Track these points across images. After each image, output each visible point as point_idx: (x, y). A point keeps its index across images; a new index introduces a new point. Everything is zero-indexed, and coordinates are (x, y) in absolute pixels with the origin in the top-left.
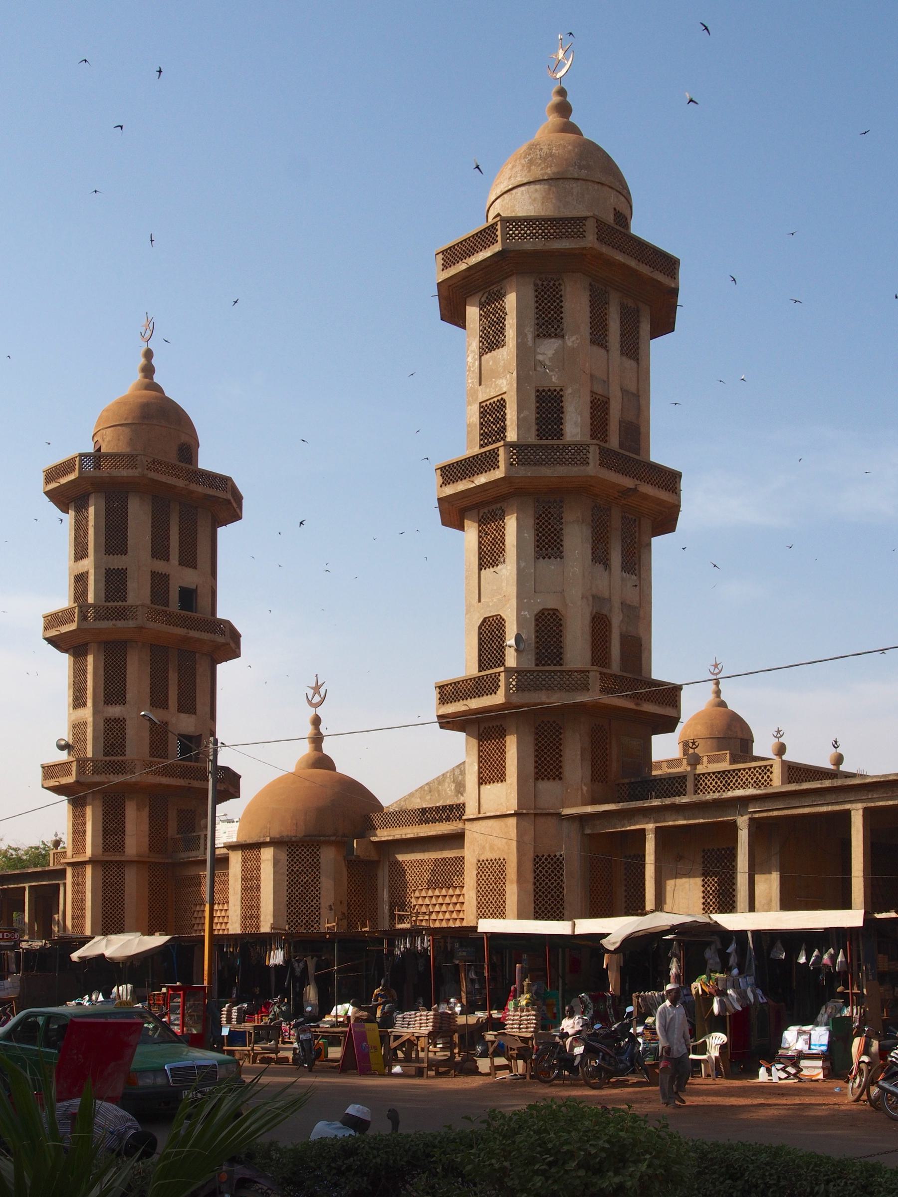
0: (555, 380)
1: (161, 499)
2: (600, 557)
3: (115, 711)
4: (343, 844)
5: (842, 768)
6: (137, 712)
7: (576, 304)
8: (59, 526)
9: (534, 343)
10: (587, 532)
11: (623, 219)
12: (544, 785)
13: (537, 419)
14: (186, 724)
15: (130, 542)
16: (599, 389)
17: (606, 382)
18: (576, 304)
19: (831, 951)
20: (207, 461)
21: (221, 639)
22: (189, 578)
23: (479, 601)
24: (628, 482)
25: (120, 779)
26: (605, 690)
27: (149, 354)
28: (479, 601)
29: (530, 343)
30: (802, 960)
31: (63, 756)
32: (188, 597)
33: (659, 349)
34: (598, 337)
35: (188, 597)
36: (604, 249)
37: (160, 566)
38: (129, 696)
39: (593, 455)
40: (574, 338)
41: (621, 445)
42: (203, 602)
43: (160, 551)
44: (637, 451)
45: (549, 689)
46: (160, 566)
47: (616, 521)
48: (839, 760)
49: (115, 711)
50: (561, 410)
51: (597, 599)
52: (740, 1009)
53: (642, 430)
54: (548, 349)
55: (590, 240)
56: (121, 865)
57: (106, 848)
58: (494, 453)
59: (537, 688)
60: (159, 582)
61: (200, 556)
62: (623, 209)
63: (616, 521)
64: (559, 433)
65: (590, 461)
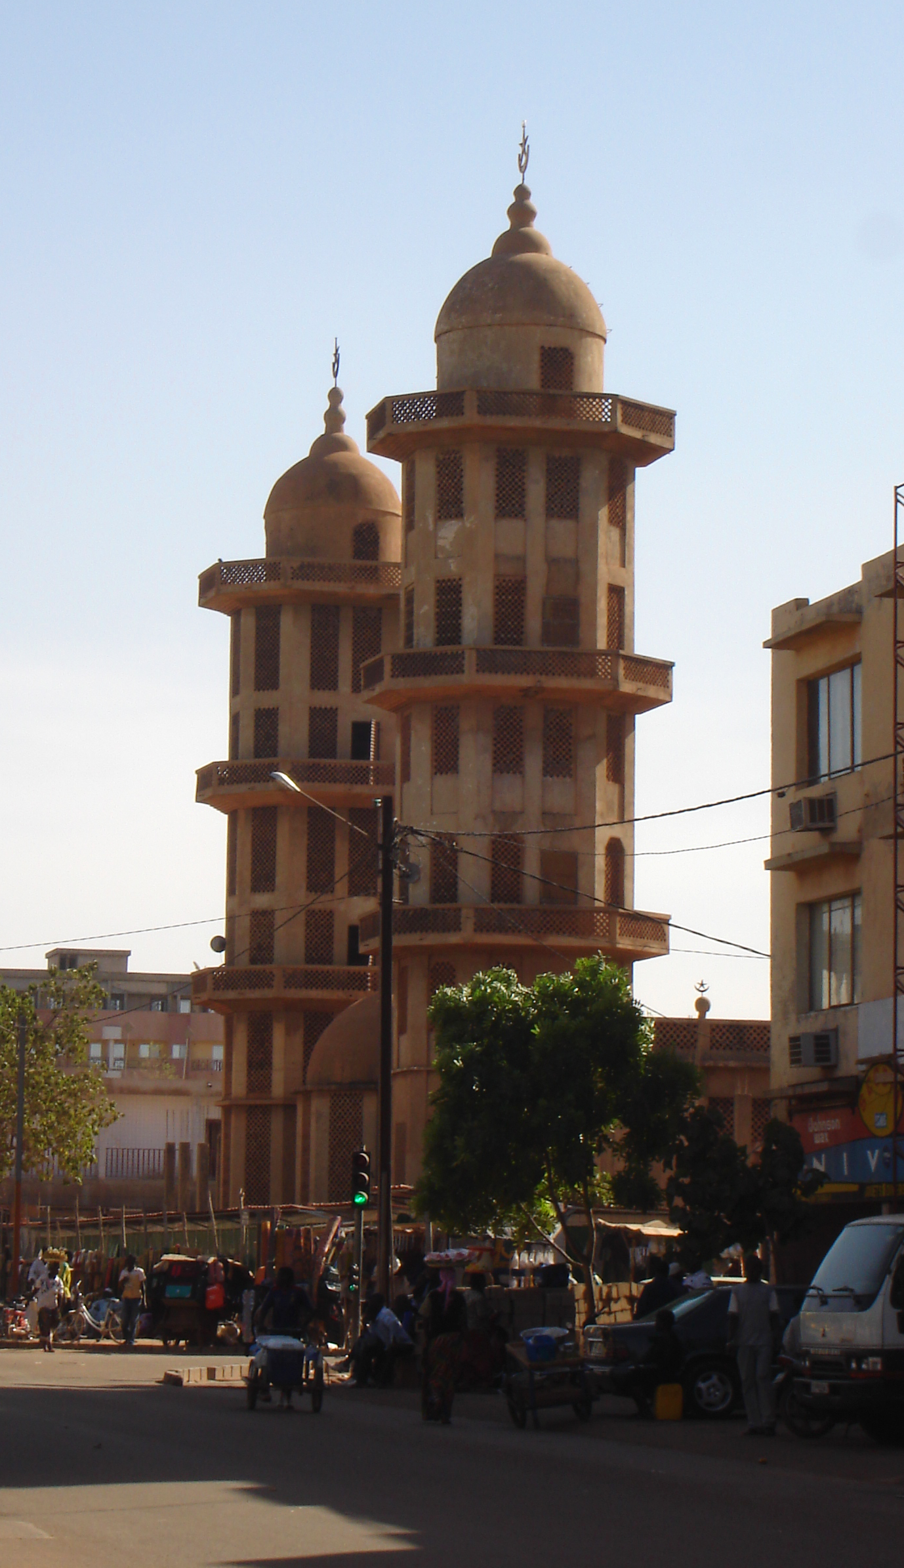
0: (453, 567)
3: (262, 900)
5: (709, 1016)
9: (436, 525)
13: (437, 614)
15: (283, 672)
19: (514, 1206)
26: (480, 928)
27: (335, 375)
29: (431, 527)
37: (324, 699)
38: (279, 879)
40: (472, 518)
46: (324, 699)
48: (703, 1005)
49: (262, 900)
51: (505, 817)
52: (425, 1259)
54: (449, 532)
56: (266, 1110)
57: (251, 1087)
60: (322, 719)
65: (466, 668)
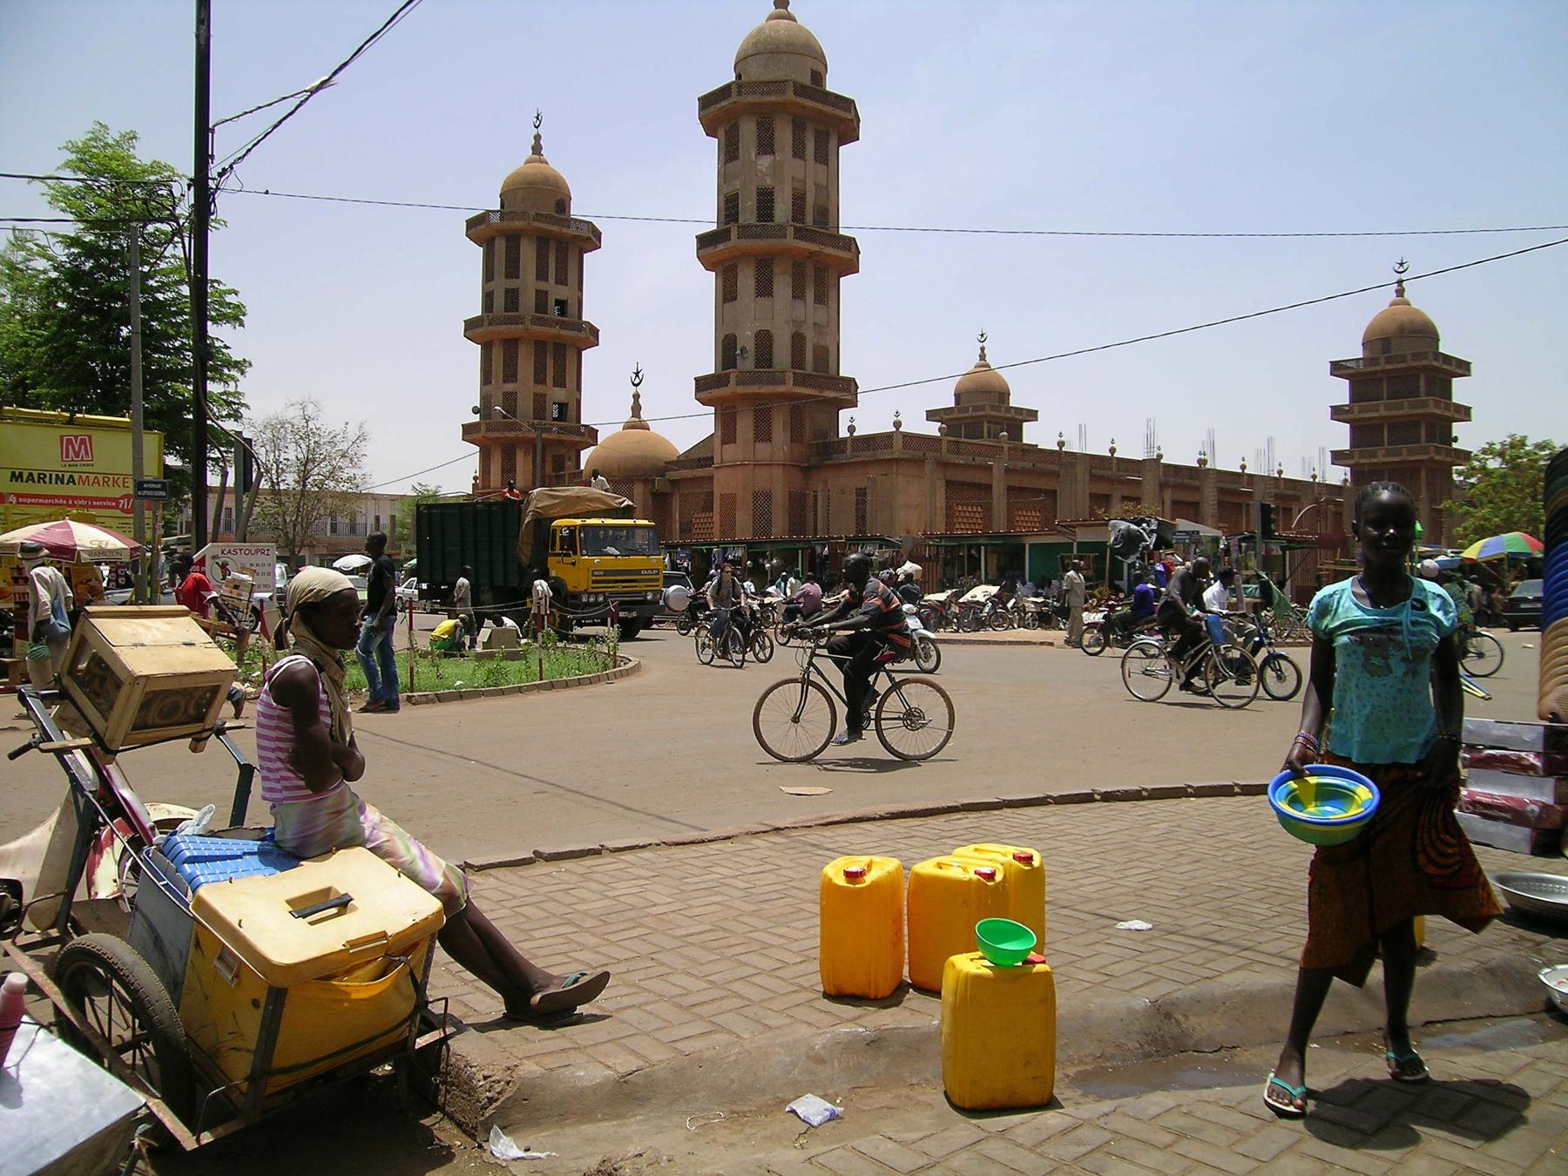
1: (543, 241)
2: (798, 294)
4: (647, 481)
6: (525, 386)
7: (784, 135)
8: (475, 254)
10: (788, 279)
11: (818, 77)
12: (759, 446)
14: (559, 394)
16: (797, 186)
17: (804, 181)
18: (784, 135)
20: (577, 210)
21: (582, 335)
22: (556, 292)
23: (13, 756)
24: (814, 247)
25: (512, 434)
28: (13, 756)
30: (150, 1047)
31: (477, 418)
32: (562, 304)
33: (847, 154)
34: (799, 153)
35: (562, 304)
36: (799, 100)
39: (790, 231)
41: (815, 222)
42: (572, 309)
43: (542, 274)
44: (825, 224)
45: (761, 383)
46: (542, 286)
47: (810, 271)
50: (772, 201)
53: (832, 209)
55: (790, 96)
58: (728, 231)
59: (752, 383)
61: (570, 274)
62: (820, 69)
63: (810, 271)
64: (771, 217)
